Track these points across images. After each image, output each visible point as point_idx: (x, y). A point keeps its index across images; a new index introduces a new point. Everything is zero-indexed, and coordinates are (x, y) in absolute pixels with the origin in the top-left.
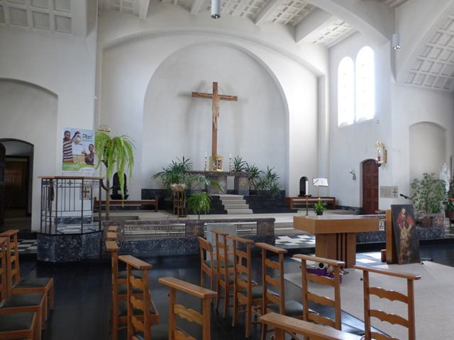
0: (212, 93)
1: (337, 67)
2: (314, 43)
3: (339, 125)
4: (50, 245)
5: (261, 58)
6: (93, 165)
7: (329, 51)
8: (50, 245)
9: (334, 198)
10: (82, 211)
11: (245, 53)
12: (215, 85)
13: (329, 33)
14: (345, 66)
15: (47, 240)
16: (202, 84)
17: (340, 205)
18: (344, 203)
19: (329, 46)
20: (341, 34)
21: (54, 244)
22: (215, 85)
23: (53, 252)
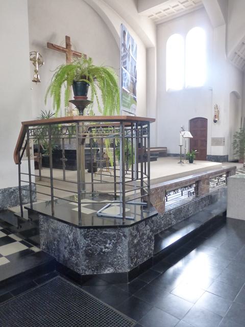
0: (65, 47)
1: (166, 41)
2: (149, 17)
3: (167, 90)
4: (115, 245)
5: (112, 23)
6: (22, 123)
7: (158, 26)
8: (115, 245)
9: (166, 148)
10: (52, 188)
11: (96, 12)
12: (68, 38)
13: (169, 9)
14: (174, 42)
15: (109, 237)
16: (54, 36)
17: (168, 153)
18: (173, 150)
19: (158, 23)
20: (176, 12)
21: (126, 242)
22: (68, 38)
23: (126, 255)
